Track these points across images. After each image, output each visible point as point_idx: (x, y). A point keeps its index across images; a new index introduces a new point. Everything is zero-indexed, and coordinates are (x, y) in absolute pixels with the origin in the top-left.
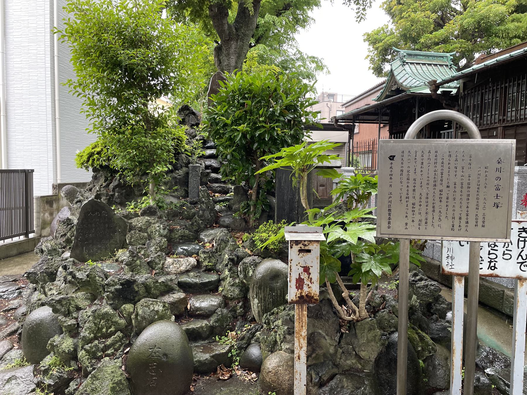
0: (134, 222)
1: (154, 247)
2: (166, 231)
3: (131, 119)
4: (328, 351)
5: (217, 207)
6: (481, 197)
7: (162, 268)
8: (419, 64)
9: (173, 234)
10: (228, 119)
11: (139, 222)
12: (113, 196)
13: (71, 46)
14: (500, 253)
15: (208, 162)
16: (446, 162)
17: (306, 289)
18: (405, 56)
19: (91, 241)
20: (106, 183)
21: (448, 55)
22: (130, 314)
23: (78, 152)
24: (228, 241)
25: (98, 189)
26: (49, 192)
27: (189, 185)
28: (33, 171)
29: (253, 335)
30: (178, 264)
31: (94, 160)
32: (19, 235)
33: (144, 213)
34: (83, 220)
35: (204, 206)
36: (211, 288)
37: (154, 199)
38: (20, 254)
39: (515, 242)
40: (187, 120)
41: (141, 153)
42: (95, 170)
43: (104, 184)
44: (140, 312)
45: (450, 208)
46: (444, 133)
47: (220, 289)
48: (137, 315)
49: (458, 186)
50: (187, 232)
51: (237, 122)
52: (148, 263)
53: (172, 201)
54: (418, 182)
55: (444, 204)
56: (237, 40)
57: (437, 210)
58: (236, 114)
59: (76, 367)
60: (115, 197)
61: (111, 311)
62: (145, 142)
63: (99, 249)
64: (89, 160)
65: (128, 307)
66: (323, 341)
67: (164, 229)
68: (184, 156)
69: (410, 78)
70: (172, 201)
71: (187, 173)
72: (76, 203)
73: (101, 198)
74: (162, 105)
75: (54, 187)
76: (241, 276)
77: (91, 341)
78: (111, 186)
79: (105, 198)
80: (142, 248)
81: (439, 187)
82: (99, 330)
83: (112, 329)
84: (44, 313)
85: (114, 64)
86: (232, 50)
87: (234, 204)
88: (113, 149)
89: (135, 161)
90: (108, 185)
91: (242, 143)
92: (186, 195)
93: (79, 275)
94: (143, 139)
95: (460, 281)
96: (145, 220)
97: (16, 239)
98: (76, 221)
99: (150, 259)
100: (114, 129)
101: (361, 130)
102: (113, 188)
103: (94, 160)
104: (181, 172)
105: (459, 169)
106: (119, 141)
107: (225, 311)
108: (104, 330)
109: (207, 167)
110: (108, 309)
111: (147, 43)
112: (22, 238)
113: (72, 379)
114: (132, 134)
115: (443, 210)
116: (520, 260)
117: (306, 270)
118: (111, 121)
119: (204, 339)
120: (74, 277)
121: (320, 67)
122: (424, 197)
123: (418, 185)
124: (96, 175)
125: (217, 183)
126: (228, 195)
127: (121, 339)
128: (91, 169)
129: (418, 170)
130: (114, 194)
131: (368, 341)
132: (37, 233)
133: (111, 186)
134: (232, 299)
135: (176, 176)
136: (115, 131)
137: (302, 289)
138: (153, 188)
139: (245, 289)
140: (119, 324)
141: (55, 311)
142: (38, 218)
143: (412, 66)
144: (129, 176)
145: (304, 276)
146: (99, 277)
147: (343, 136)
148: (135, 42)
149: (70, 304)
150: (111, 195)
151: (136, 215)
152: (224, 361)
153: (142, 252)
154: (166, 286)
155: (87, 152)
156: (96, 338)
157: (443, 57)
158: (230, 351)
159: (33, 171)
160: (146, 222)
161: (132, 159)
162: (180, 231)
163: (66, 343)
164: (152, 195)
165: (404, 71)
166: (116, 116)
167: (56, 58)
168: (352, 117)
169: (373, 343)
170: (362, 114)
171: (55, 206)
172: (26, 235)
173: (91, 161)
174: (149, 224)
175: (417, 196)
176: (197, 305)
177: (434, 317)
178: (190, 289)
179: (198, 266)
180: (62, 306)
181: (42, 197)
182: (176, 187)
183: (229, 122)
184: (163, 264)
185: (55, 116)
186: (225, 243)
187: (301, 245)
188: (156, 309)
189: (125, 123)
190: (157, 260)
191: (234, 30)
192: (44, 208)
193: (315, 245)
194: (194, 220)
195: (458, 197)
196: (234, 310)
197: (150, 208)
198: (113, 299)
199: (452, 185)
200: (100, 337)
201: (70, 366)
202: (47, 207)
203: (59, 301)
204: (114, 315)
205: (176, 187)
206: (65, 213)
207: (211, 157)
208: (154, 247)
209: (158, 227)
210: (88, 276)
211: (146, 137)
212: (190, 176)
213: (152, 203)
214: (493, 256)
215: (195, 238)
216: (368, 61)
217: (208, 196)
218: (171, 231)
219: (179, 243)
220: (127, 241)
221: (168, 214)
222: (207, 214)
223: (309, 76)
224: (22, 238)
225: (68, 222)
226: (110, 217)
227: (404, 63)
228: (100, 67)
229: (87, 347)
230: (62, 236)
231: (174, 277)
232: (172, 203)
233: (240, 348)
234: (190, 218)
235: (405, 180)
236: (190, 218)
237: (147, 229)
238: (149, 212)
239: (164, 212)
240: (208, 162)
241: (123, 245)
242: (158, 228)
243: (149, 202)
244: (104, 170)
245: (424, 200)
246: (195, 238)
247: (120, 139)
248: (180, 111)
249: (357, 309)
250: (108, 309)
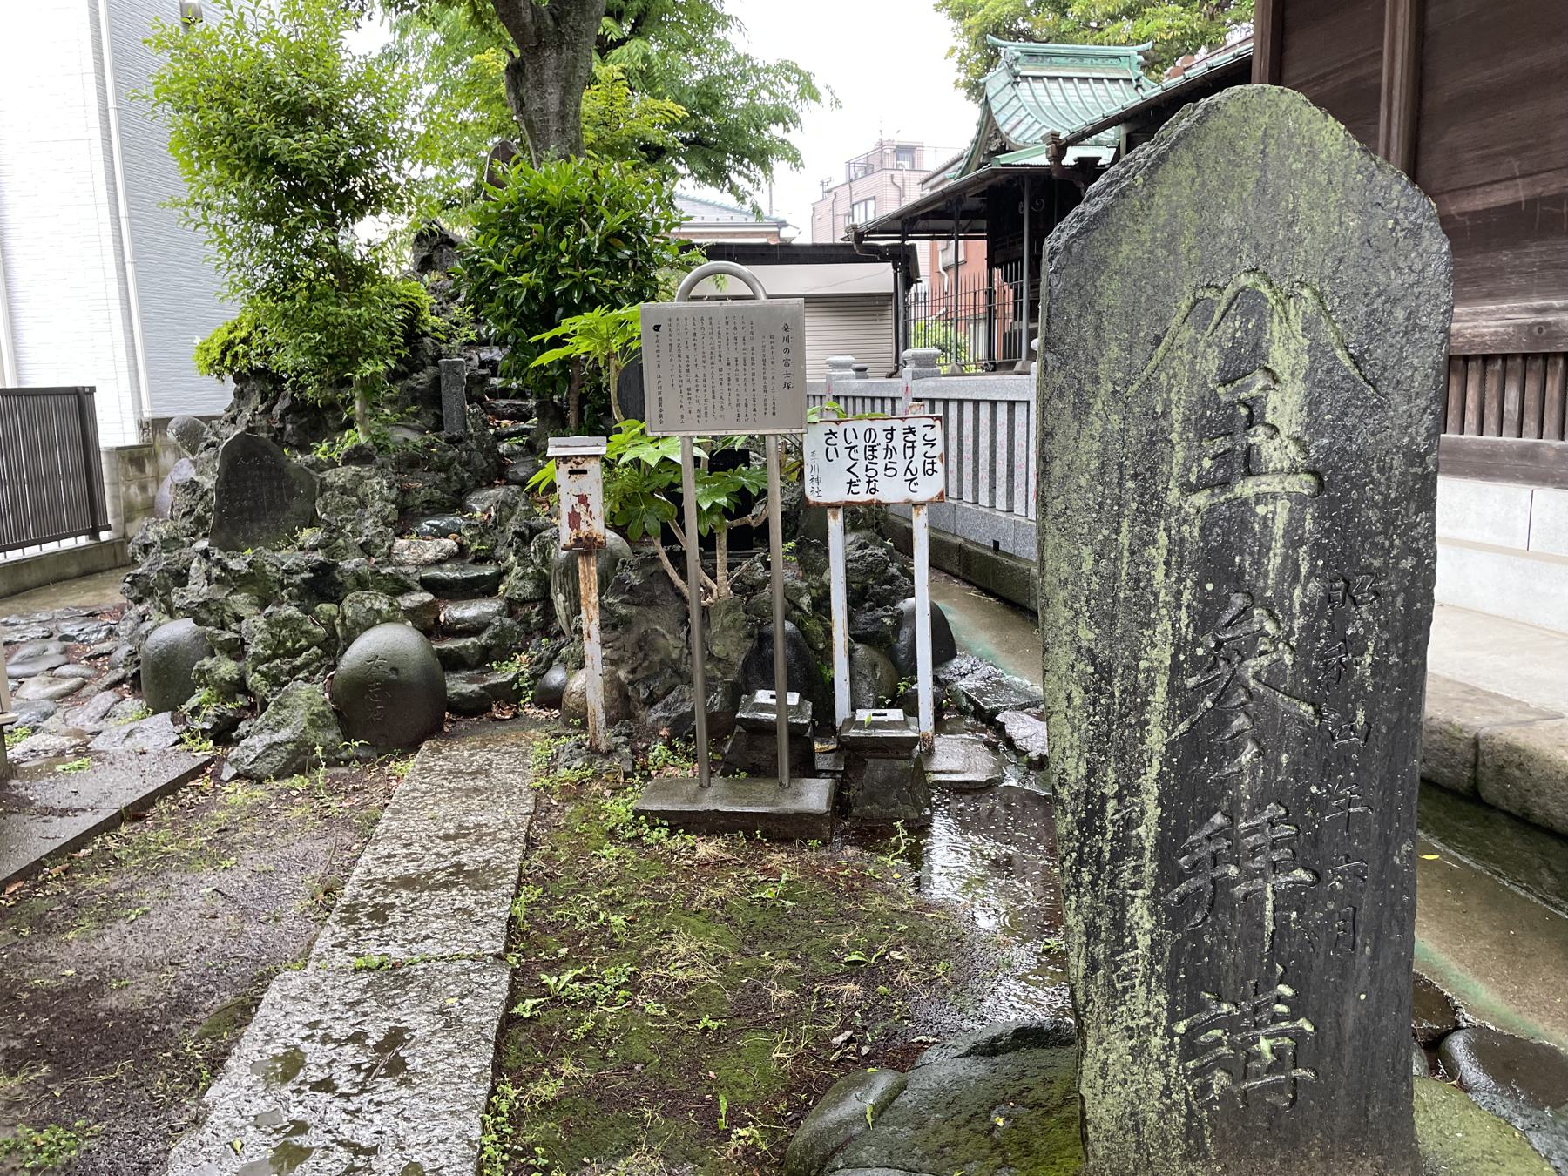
0: (330, 476)
2: (395, 492)
3: (306, 266)
4: (669, 655)
5: (503, 447)
6: (769, 376)
7: (389, 555)
8: (1056, 78)
9: (409, 498)
13: (167, 124)
14: (880, 468)
16: (723, 331)
17: (584, 527)
18: (1017, 59)
19: (246, 515)
21: (1132, 50)
22: (331, 618)
23: (198, 340)
24: (516, 504)
26: (132, 439)
28: (93, 389)
29: (556, 652)
30: (419, 550)
31: (235, 357)
32: (75, 535)
33: (348, 460)
34: (227, 473)
35: (473, 444)
36: (486, 587)
37: (367, 432)
38: (87, 574)
39: (900, 449)
40: (436, 258)
41: (331, 337)
42: (238, 378)
43: (261, 408)
44: (349, 613)
45: (733, 393)
47: (502, 587)
48: (344, 618)
49: (741, 361)
50: (437, 493)
51: (518, 266)
52: (361, 546)
53: (407, 437)
54: (692, 359)
55: (725, 386)
56: (560, 46)
57: (718, 396)
58: (515, 252)
59: (246, 703)
61: (299, 614)
62: (337, 315)
63: (263, 529)
64: (225, 358)
65: (328, 608)
66: (661, 641)
67: (390, 488)
68: (427, 340)
69: (1029, 120)
70: (407, 437)
72: (207, 447)
74: (367, 232)
75: (143, 427)
76: (537, 561)
77: (268, 660)
78: (277, 410)
80: (348, 520)
81: (717, 366)
82: (281, 643)
83: (303, 642)
84: (181, 629)
85: (261, 162)
86: (549, 73)
88: (276, 333)
89: (320, 354)
90: (268, 410)
91: (529, 309)
92: (438, 426)
93: (233, 564)
94: (333, 309)
95: (835, 515)
97: (68, 543)
98: (208, 483)
99: (363, 539)
100: (273, 291)
101: (972, 255)
103: (235, 357)
104: (424, 377)
105: (740, 340)
106: (285, 315)
107: (508, 621)
108: (289, 644)
109: (483, 364)
110: (291, 611)
111: (325, 114)
112: (83, 541)
113: (242, 719)
114: (310, 299)
115: (726, 397)
116: (909, 476)
117: (583, 499)
118: (263, 276)
119: (471, 668)
120: (225, 568)
121: (809, 91)
122: (701, 378)
123: (692, 363)
125: (506, 398)
127: (319, 658)
128: (229, 378)
129: (691, 343)
131: (724, 629)
132: (116, 531)
133: (277, 410)
134: (524, 602)
136: (275, 294)
137: (578, 528)
138: (363, 410)
139: (543, 583)
140: (314, 635)
141: (199, 622)
142: (115, 497)
143: (1038, 86)
145: (580, 509)
146: (272, 565)
147: (878, 277)
148: (296, 114)
149: (224, 611)
152: (509, 695)
153: (349, 527)
154: (397, 581)
155: (218, 341)
156: (275, 656)
157: (1117, 57)
158: (515, 679)
159: (93, 389)
161: (314, 351)
163: (227, 668)
164: (362, 423)
165: (1015, 101)
166: (277, 265)
167: (112, 113)
168: (898, 225)
169: (732, 632)
170: (925, 217)
171: (149, 469)
172: (94, 534)
173: (228, 362)
175: (693, 379)
176: (457, 614)
177: (867, 605)
178: (445, 590)
179: (460, 554)
180: (210, 612)
181: (118, 449)
182: (413, 408)
183: (501, 268)
184: (390, 547)
187: (571, 463)
188: (376, 606)
189: (294, 279)
190: (377, 541)
191: (550, 22)
192: (126, 474)
193: (593, 461)
195: (741, 377)
196: (525, 621)
197: (358, 448)
198: (300, 598)
199: (733, 362)
200: (283, 656)
201: (235, 701)
202: (132, 472)
203: (205, 604)
204: (302, 621)
205: (413, 408)
206: (184, 470)
209: (377, 484)
210: (250, 564)
211: (339, 305)
212: (443, 384)
213: (363, 440)
214: (872, 473)
215: (457, 504)
216: (953, 63)
217: (486, 424)
218: (404, 492)
219: (423, 515)
221: (398, 462)
222: (479, 459)
223: (778, 117)
224: (83, 541)
225: (192, 487)
226: (279, 471)
227: (1016, 79)
228: (237, 167)
229: (262, 668)
230: (184, 515)
231: (412, 570)
232: (406, 440)
233: (535, 676)
234: (444, 467)
235: (676, 358)
236: (444, 467)
238: (358, 456)
240: (486, 355)
241: (312, 521)
243: (357, 437)
244: (258, 380)
245: (701, 383)
246: (457, 504)
247: (287, 310)
248: (420, 238)
249: (715, 587)
250: (291, 611)
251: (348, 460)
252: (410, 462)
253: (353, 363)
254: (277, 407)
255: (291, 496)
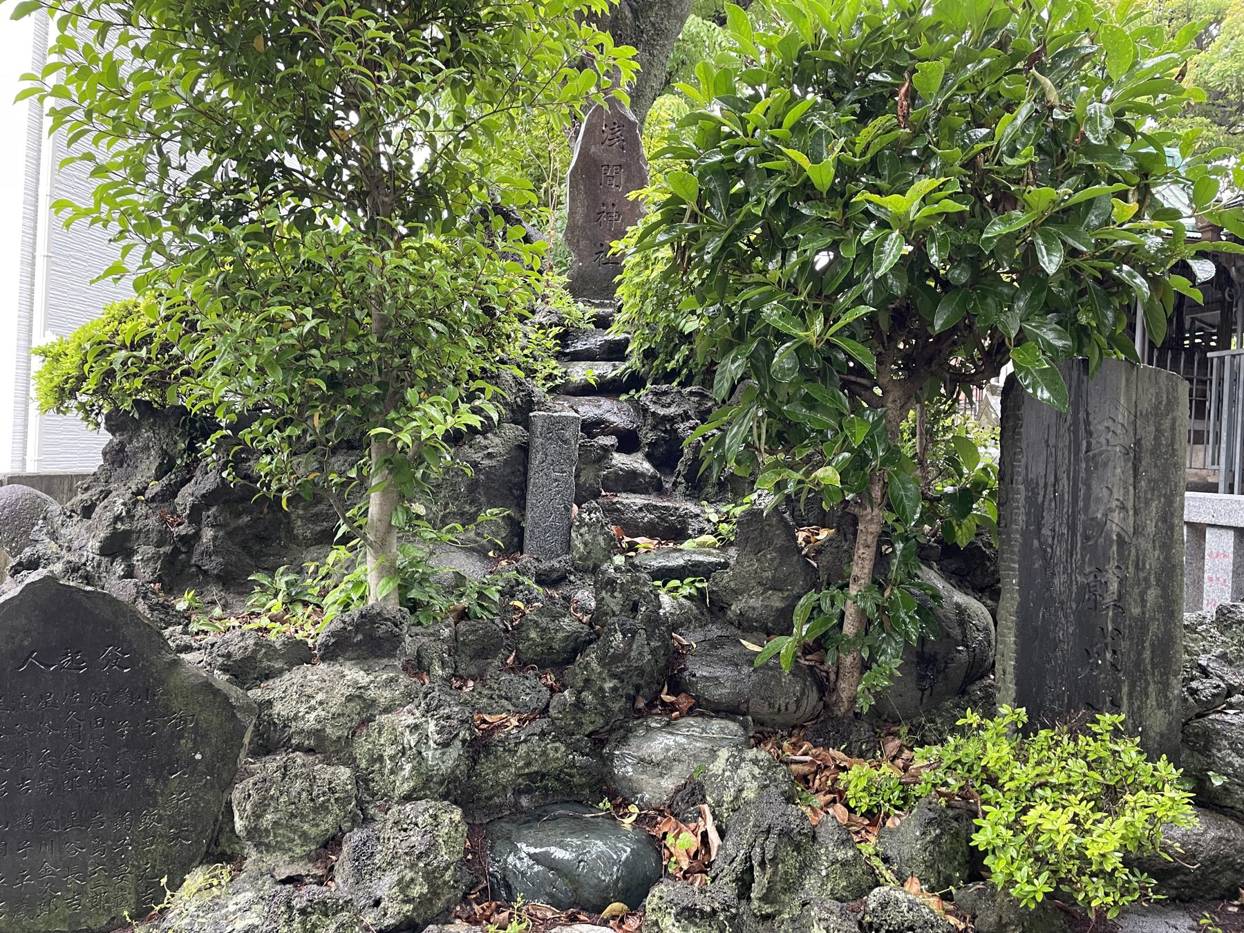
1: (391, 878)
2: (456, 750)
9: (485, 767)
10: (816, 159)
11: (308, 695)
12: (189, 541)
15: (589, 409)
20: (165, 481)
25: (119, 508)
27: (531, 500)
33: (337, 648)
37: (389, 570)
41: (344, 322)
42: (116, 423)
43: (155, 487)
46: (1222, 359)
60: (199, 549)
71: (523, 451)
73: (133, 552)
78: (186, 497)
79: (150, 550)
87: (736, 593)
89: (308, 371)
90: (170, 493)
92: (515, 542)
96: (342, 691)
102: (193, 507)
124: (122, 445)
126: (688, 545)
130: (197, 536)
133: (186, 497)
135: (477, 457)
138: (387, 515)
144: (268, 451)
150: (183, 539)
151: (299, 654)
160: (350, 699)
161: (294, 360)
162: (523, 749)
164: (381, 546)
174: (365, 710)
185: (34, 249)
186: (798, 848)
194: (576, 674)
207: (607, 388)
208: (391, 878)
212: (536, 459)
213: (380, 592)
220: (239, 824)
232: (460, 579)
236: (559, 659)
237: (349, 741)
238: (364, 639)
239: (436, 636)
242: (411, 739)
251: (337, 648)
252: (481, 646)
253: (392, 398)
254: (187, 489)
255: (163, 769)
